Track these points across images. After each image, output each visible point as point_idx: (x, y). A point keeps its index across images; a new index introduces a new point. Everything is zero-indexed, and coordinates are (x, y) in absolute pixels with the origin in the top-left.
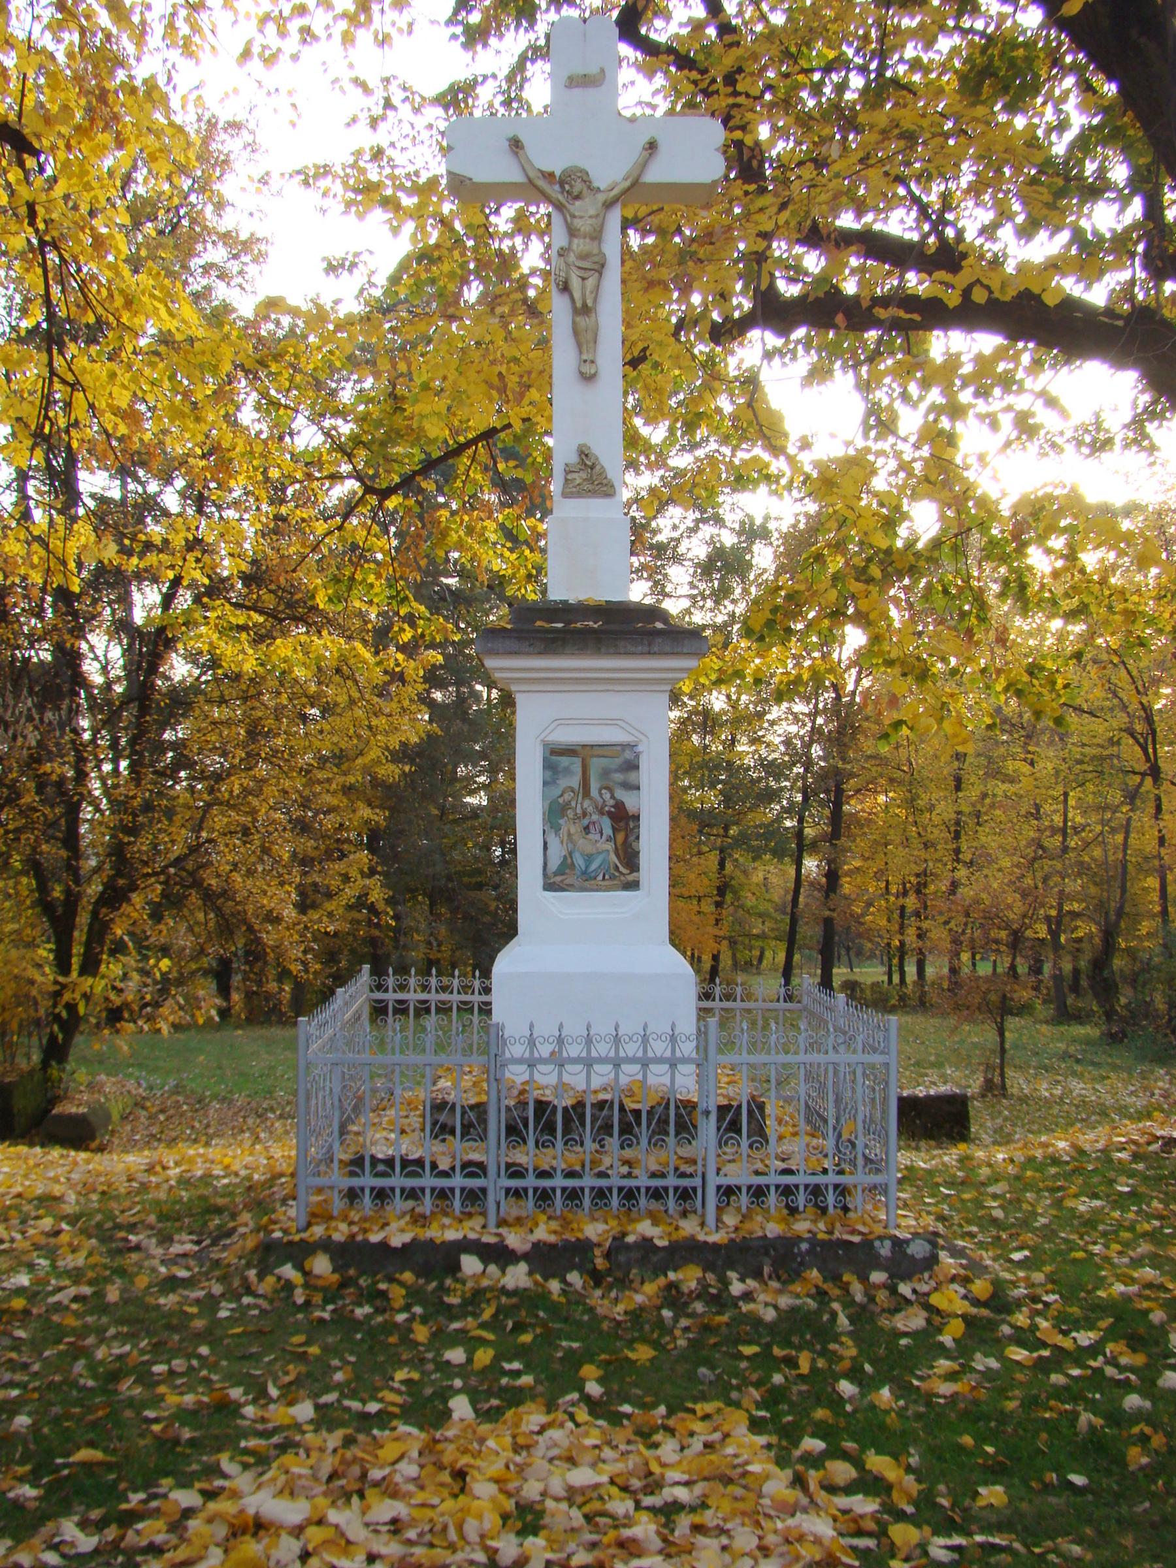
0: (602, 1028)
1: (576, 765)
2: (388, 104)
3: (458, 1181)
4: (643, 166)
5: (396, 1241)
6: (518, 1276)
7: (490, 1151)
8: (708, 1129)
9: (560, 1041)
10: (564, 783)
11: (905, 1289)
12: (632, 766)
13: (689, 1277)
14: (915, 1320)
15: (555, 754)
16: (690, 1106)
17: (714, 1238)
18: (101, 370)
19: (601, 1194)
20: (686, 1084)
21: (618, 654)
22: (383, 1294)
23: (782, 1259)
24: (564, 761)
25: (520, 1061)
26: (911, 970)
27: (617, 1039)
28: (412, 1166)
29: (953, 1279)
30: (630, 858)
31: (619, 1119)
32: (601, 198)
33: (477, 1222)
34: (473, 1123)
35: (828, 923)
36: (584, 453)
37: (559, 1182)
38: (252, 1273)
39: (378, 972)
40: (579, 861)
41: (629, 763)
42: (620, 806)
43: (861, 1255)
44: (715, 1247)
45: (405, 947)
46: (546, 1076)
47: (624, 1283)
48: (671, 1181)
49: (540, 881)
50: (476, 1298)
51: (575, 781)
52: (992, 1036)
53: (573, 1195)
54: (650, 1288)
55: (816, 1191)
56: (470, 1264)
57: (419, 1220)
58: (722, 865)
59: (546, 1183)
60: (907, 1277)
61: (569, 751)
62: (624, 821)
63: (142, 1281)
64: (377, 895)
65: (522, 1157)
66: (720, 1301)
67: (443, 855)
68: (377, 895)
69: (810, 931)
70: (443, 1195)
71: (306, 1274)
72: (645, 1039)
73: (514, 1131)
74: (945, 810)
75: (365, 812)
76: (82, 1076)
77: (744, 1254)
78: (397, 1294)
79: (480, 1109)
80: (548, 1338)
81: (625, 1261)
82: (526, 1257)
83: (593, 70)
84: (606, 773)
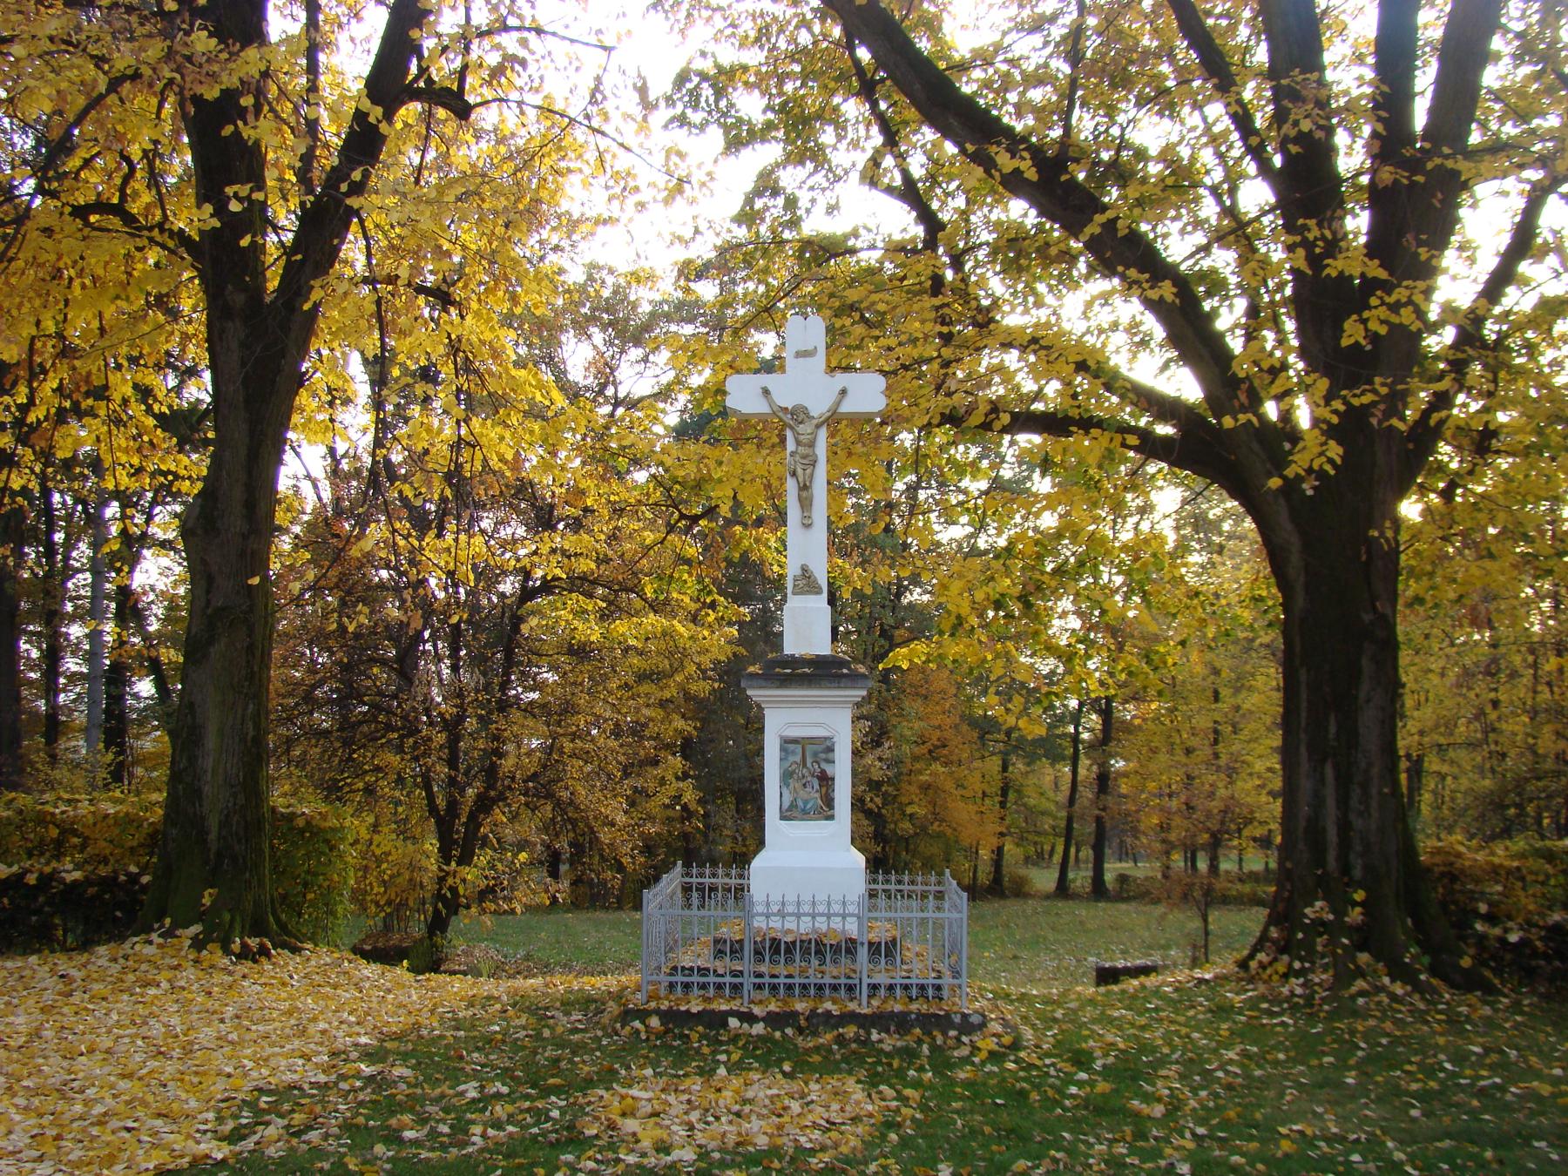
0: (806, 897)
1: (799, 749)
2: (697, 231)
3: (728, 979)
4: (838, 403)
5: (694, 1010)
6: (759, 1029)
7: (746, 964)
8: (863, 953)
9: (783, 904)
10: (791, 759)
11: (965, 1039)
12: (831, 750)
13: (850, 1031)
14: (965, 1051)
15: (787, 743)
16: (853, 941)
17: (865, 1011)
18: (494, 433)
19: (804, 987)
20: (852, 927)
21: (821, 688)
22: (688, 1036)
23: (901, 1023)
24: (791, 747)
25: (762, 914)
26: (1202, 865)
27: (799, 904)
28: (703, 971)
29: (994, 1035)
30: (829, 802)
31: (816, 948)
32: (815, 422)
33: (738, 1002)
34: (736, 949)
35: (1099, 820)
36: (804, 569)
37: (782, 980)
38: (618, 1025)
39: (687, 865)
40: (800, 804)
41: (826, 748)
42: (823, 772)
43: (943, 1022)
44: (865, 1015)
45: (714, 842)
46: (775, 923)
47: (815, 1034)
48: (843, 981)
49: (778, 816)
50: (734, 1039)
51: (798, 758)
52: (1197, 923)
53: (789, 987)
54: (829, 1036)
55: (922, 987)
56: (733, 1022)
57: (707, 1000)
58: (1005, 768)
59: (776, 981)
60: (968, 1034)
61: (795, 741)
62: (826, 781)
63: (560, 1030)
64: (690, 796)
65: (763, 968)
66: (866, 1042)
67: (747, 759)
68: (690, 796)
69: (1084, 829)
70: (719, 987)
71: (647, 1026)
72: (829, 904)
73: (758, 953)
74: (1203, 722)
75: (679, 723)
76: (461, 945)
77: (879, 1020)
78: (695, 1036)
79: (741, 942)
80: (770, 1052)
81: (818, 1022)
82: (763, 1019)
83: (810, 348)
84: (815, 754)
